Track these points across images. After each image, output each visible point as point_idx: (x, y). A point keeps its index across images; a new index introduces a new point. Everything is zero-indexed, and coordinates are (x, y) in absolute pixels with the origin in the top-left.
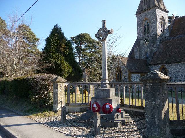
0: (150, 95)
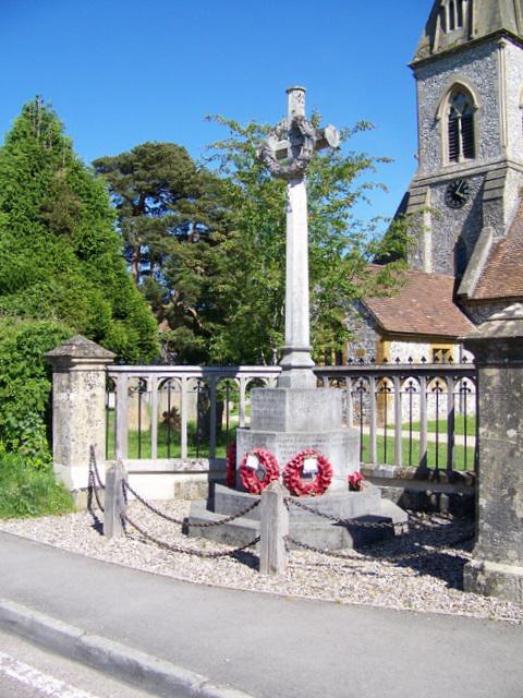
0: (497, 404)
